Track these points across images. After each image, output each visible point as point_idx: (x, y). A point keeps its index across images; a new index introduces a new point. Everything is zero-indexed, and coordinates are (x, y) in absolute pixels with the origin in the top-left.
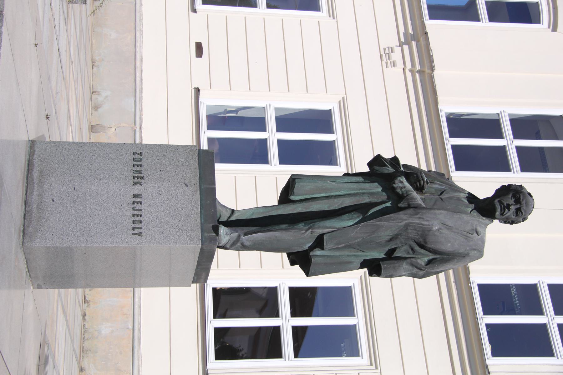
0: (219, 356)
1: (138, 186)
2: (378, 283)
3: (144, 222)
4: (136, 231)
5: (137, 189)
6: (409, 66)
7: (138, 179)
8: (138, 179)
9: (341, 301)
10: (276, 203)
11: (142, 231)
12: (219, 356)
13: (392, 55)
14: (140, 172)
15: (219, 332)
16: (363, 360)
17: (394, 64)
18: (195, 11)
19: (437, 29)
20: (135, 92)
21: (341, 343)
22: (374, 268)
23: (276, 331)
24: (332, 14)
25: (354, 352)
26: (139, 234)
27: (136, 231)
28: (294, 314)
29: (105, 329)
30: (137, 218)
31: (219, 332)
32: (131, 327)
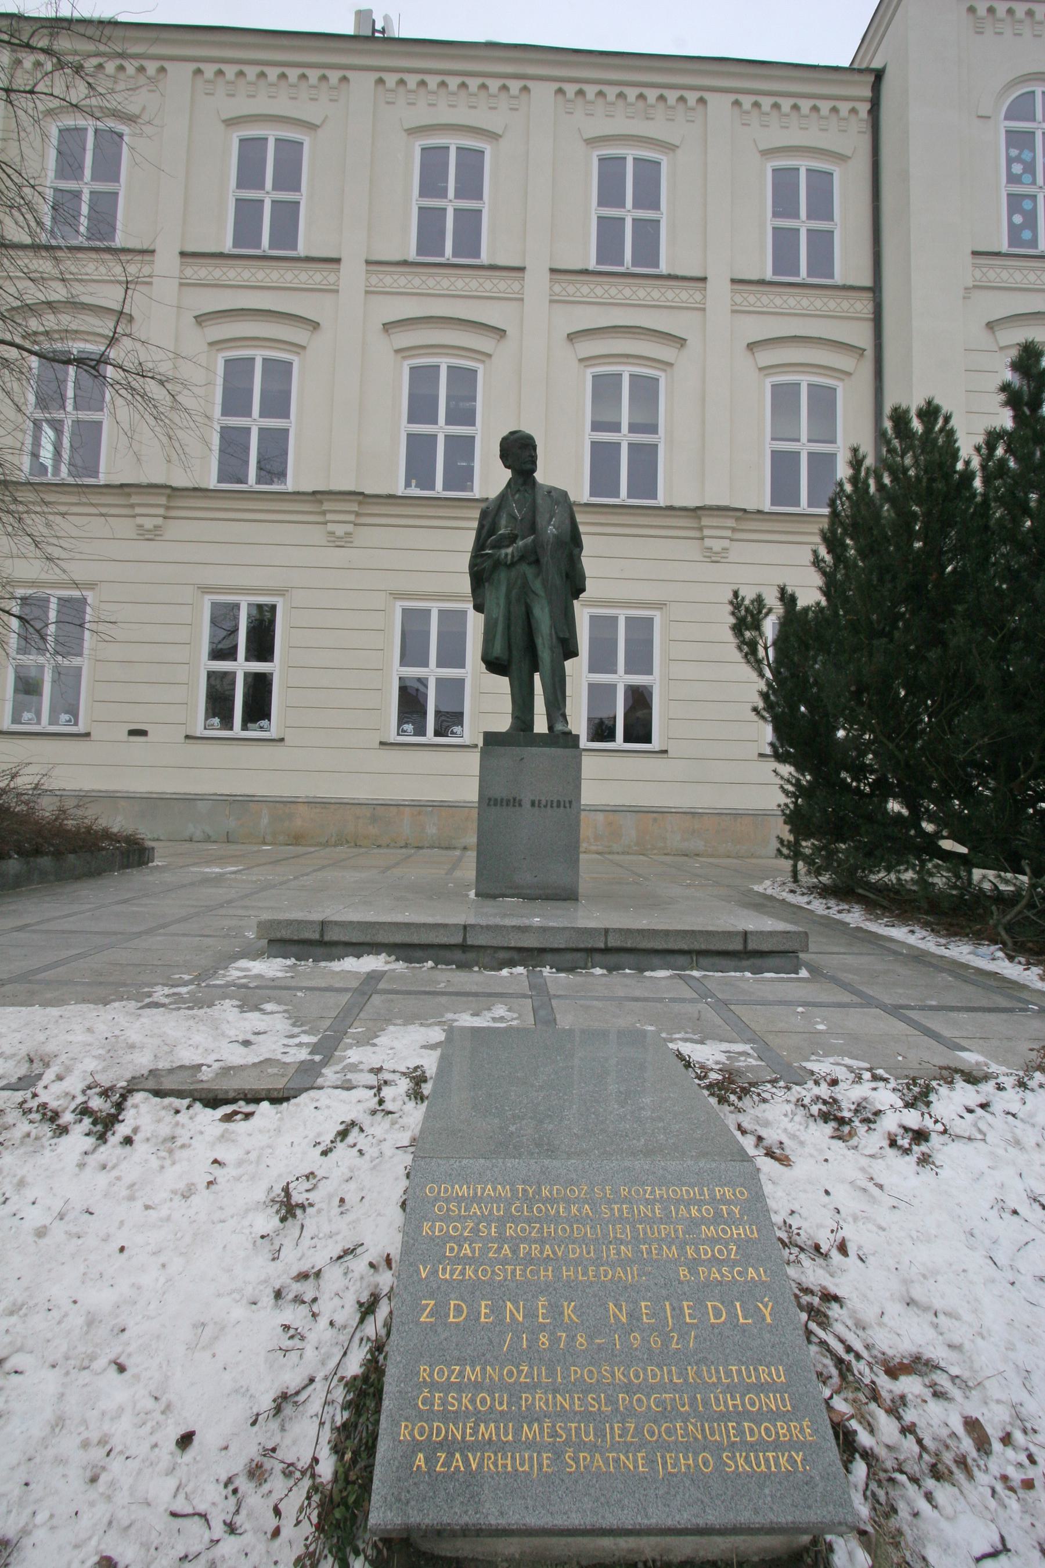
0: (648, 740)
1: (523, 803)
2: (592, 588)
3: (560, 798)
4: (567, 805)
5: (527, 804)
6: (352, 518)
7: (515, 802)
8: (515, 802)
9: (603, 626)
10: (507, 679)
11: (567, 800)
12: (648, 740)
13: (338, 534)
14: (508, 801)
15: (627, 739)
16: (657, 616)
17: (725, 549)
18: (88, 735)
19: (298, 477)
20: (190, 800)
21: (641, 633)
22: (578, 589)
23: (439, 681)
24: (92, 586)
25: (273, 608)
26: (570, 802)
27: (567, 805)
28: (426, 665)
29: (432, 830)
30: (555, 804)
31: (627, 739)
32: (430, 809)
